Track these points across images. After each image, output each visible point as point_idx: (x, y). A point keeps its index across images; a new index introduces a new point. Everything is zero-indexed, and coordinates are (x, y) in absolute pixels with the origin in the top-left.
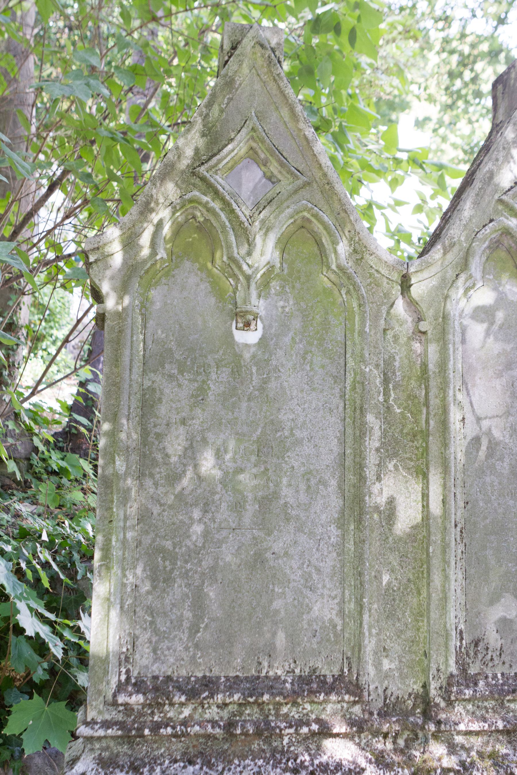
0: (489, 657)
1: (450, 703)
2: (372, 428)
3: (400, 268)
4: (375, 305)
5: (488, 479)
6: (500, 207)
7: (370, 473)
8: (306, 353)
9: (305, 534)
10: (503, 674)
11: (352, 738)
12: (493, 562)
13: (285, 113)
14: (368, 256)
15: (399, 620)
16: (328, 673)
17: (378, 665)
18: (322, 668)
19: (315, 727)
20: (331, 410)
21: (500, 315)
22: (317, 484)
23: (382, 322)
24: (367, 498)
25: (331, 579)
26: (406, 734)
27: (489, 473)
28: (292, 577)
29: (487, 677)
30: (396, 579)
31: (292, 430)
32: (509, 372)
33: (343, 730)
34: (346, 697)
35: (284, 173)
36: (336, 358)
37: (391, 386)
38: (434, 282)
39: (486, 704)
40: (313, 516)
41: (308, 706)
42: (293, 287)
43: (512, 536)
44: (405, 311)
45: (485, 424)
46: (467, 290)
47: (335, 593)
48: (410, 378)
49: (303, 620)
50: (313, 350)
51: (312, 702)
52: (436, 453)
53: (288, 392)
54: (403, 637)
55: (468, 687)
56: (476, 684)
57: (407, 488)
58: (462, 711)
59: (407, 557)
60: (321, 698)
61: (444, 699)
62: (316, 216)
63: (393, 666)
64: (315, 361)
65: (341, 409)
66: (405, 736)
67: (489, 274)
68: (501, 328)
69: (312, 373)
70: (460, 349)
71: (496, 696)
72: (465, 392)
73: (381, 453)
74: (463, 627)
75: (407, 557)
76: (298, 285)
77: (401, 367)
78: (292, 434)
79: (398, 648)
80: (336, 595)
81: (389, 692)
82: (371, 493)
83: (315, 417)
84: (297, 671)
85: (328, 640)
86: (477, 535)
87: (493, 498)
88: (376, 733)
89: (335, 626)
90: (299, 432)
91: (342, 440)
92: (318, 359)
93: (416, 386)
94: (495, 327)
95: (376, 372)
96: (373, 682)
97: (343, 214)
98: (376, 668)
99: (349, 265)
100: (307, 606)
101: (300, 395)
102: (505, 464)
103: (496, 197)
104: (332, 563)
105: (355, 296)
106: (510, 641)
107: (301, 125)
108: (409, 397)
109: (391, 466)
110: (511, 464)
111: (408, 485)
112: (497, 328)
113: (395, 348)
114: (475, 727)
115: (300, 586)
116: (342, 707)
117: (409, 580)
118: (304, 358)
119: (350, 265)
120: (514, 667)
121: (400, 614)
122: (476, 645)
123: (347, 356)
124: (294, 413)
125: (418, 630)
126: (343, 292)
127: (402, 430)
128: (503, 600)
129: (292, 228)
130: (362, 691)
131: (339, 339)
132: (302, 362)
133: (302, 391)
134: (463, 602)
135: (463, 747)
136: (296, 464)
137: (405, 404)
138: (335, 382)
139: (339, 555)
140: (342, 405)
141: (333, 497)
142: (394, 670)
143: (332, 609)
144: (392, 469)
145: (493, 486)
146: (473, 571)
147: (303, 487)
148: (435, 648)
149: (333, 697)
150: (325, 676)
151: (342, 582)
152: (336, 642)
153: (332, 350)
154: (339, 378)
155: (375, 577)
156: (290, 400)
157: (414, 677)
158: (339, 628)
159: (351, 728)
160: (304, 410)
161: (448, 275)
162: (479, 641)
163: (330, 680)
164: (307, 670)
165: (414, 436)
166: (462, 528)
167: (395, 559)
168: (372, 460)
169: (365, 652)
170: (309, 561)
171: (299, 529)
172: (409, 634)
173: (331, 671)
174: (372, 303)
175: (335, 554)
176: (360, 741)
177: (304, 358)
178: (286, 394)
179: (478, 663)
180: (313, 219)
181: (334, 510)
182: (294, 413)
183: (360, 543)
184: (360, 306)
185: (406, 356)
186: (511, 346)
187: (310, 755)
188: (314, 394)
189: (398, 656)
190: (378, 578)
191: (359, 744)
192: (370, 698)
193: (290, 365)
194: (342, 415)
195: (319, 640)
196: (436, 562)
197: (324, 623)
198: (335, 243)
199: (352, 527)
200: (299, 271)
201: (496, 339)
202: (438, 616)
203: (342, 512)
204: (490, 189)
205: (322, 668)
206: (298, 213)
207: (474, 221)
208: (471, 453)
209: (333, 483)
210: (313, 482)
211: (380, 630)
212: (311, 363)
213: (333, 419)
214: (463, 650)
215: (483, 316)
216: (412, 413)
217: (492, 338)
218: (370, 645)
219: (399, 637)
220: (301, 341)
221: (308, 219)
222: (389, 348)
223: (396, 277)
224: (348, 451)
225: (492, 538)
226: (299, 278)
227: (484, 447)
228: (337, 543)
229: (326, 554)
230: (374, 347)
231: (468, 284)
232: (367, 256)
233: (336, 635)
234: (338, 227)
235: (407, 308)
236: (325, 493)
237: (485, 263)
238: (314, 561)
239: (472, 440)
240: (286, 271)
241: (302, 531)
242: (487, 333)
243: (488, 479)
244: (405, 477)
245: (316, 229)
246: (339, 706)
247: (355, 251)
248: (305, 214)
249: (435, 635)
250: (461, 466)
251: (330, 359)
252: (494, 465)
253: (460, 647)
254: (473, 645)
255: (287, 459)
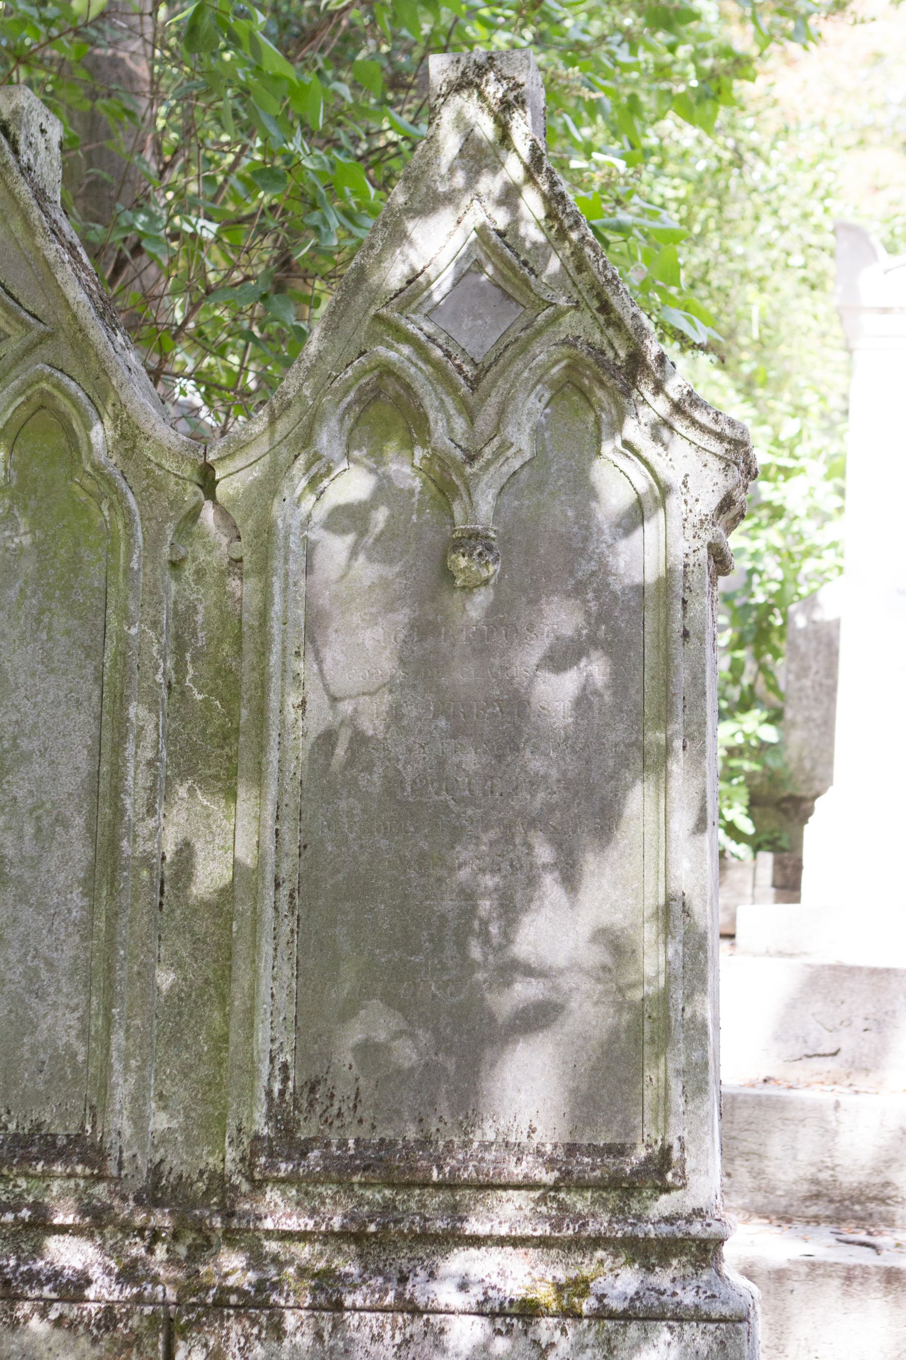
0: (334, 1111)
1: (258, 1186)
2: (142, 728)
3: (192, 456)
4: (153, 523)
5: (343, 805)
6: (380, 328)
7: (133, 803)
8: (42, 612)
9: (31, 906)
10: (357, 1141)
11: (91, 1237)
12: (347, 947)
13: (16, 225)
14: (143, 442)
15: (187, 1047)
16: (60, 1131)
17: (139, 1119)
18: (52, 1123)
19: (25, 1214)
20: (78, 703)
21: (381, 516)
22: (51, 825)
23: (166, 550)
24: (125, 843)
25: (71, 979)
26: (190, 1237)
27: (345, 793)
28: (9, 976)
29: (328, 1145)
30: (185, 979)
31: (15, 739)
32: (390, 615)
33: (69, 1220)
34: (79, 1169)
35: (13, 323)
36: (90, 616)
37: (188, 656)
38: (256, 472)
39: (321, 1189)
40: (44, 877)
41: (23, 1183)
42: (25, 508)
43: (383, 902)
44: (218, 527)
45: (346, 707)
46: (313, 483)
47: (76, 1001)
48: (221, 641)
49: (23, 1045)
50: (53, 606)
51: (27, 1176)
52: (250, 765)
53: (11, 679)
54: (193, 1075)
55: (288, 1159)
56: (304, 1155)
57: (209, 826)
58: (279, 1201)
59: (204, 942)
60: (39, 1167)
61: (247, 1179)
62: (57, 386)
63: (174, 1124)
64: (55, 625)
65: (95, 699)
66: (189, 1241)
67: (359, 448)
68: (377, 540)
69: (50, 644)
70: (302, 583)
71: (334, 1175)
72: (310, 657)
73: (157, 769)
74: (289, 1058)
75: (204, 942)
76: (32, 504)
77: (207, 622)
78: (15, 746)
79: (184, 1094)
80: (77, 1005)
81: (165, 1168)
82: (136, 835)
83: (53, 716)
84: (12, 1127)
85: (62, 1078)
86: (320, 902)
87: (351, 836)
88: (126, 1228)
89: (74, 1055)
90: (26, 741)
91: (96, 752)
92: (61, 621)
93: (231, 653)
94: (369, 540)
95: (151, 634)
96: (130, 1147)
97: (103, 378)
98: (135, 1123)
99: (113, 463)
100: (31, 1022)
101: (30, 682)
102: (375, 778)
103: (372, 312)
104: (72, 953)
105: (120, 512)
106: (373, 1083)
107: (39, 241)
108: (218, 671)
109: (182, 791)
110: (385, 777)
111: (211, 821)
112: (371, 541)
113: (198, 592)
114: (293, 1224)
115: (20, 990)
116: (77, 1185)
117: (207, 981)
118: (38, 621)
119: (113, 461)
120: (378, 1130)
121: (189, 1038)
122: (313, 1090)
123: (109, 611)
124: (19, 711)
125: (220, 1064)
126: (105, 506)
127: (204, 729)
128: (362, 1012)
129: (25, 412)
130: (104, 1159)
131: (96, 584)
132: (35, 627)
133: (33, 675)
134: (291, 1016)
135: (275, 1259)
136: (20, 794)
137: (211, 686)
138: (87, 656)
139: (84, 938)
140: (97, 692)
141: (78, 845)
142: (176, 1131)
143: (70, 1027)
144: (185, 795)
145: (353, 816)
146: (310, 963)
147: (29, 830)
148: (235, 1093)
149: (58, 1168)
150: (54, 1136)
151: (88, 983)
152: (75, 1082)
153: (84, 603)
154: (93, 651)
155: (139, 973)
156: (14, 691)
157: (209, 1144)
158: (80, 1058)
159: (83, 1218)
160: (35, 705)
161: (280, 457)
162: (318, 1082)
163: (61, 1142)
164: (28, 1125)
165: (224, 739)
166: (293, 890)
167: (184, 945)
168: (136, 779)
169: (112, 1095)
170: (36, 949)
171: (22, 899)
172: (204, 1071)
173: (66, 1129)
174: (149, 519)
175: (77, 938)
176: (104, 1243)
177: (38, 621)
178: (8, 681)
179: (315, 1120)
180: (56, 393)
181: (78, 867)
182: (19, 711)
183: (113, 916)
184: (126, 525)
185: (215, 604)
186: (397, 569)
187: (18, 1258)
188: (52, 678)
189: (185, 1108)
190: (145, 974)
191: (101, 1247)
192: (123, 1173)
193: (16, 633)
194: (97, 710)
195: (48, 1077)
196: (241, 948)
197: (56, 1049)
198: (88, 427)
199: (104, 894)
200: (35, 480)
201: (370, 559)
202: (242, 1039)
203: (92, 869)
204: (360, 299)
205: (52, 1123)
206: (30, 386)
207: (330, 358)
208: (315, 761)
209: (79, 821)
210: (46, 822)
211: (144, 1061)
212: (50, 628)
213: (82, 717)
214: (287, 1097)
215: (346, 522)
216: (222, 700)
217: (362, 558)
218: (122, 1088)
219: (186, 1076)
220: (34, 593)
221: (50, 394)
222: (187, 593)
223: (188, 471)
224: (104, 769)
225: (347, 905)
226: (35, 491)
227: (340, 751)
228: (81, 920)
229: (62, 937)
230: (151, 593)
231: (314, 470)
232: (141, 443)
233: (75, 1069)
234: (97, 401)
235: (220, 522)
236: (64, 839)
237: (352, 430)
238: (44, 950)
239: (318, 738)
240: (14, 482)
241: (27, 902)
242: (353, 553)
243: (343, 805)
244: (206, 807)
245: (62, 408)
246: (72, 1183)
247: (123, 436)
248: (44, 385)
249: (237, 1071)
250: (296, 783)
251: (81, 618)
252: (356, 779)
253: (282, 1093)
254: (306, 1090)
255: (5, 786)
